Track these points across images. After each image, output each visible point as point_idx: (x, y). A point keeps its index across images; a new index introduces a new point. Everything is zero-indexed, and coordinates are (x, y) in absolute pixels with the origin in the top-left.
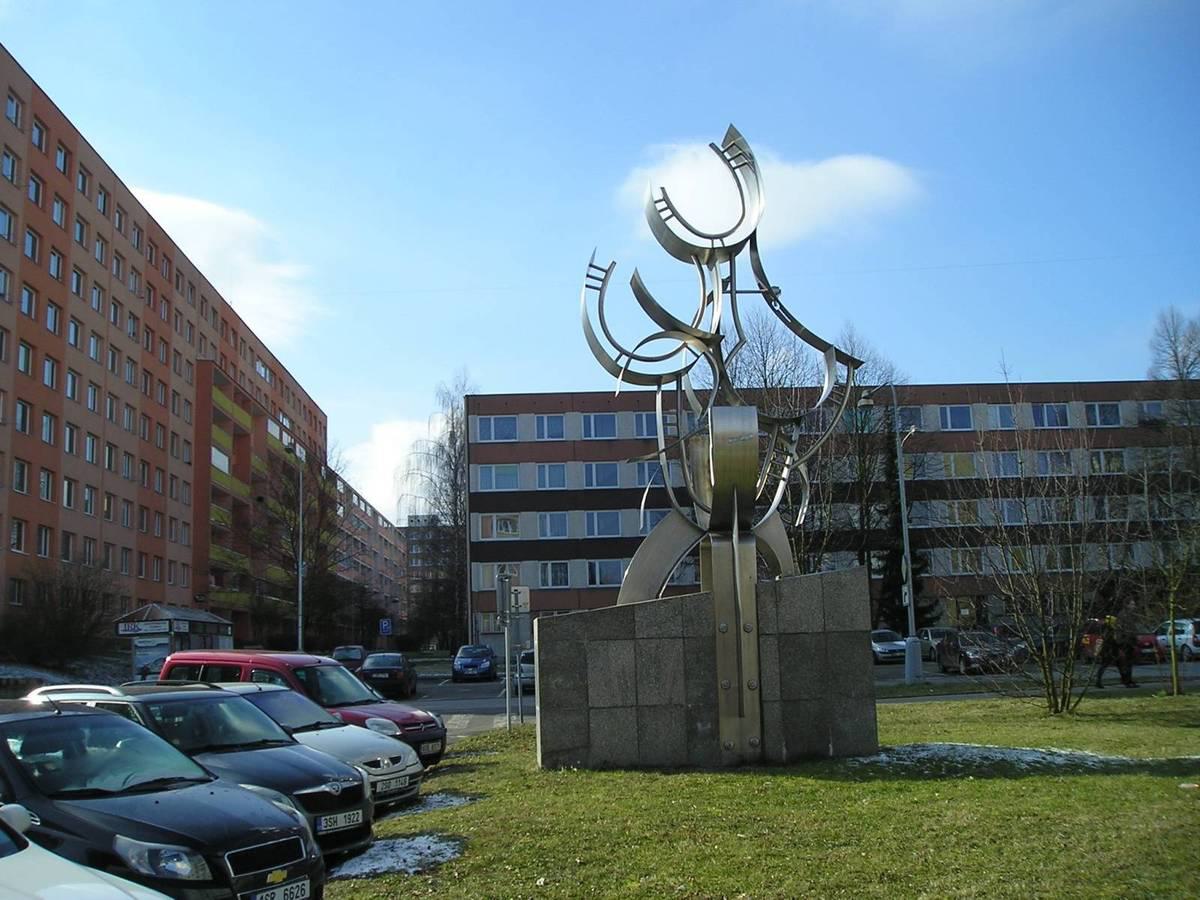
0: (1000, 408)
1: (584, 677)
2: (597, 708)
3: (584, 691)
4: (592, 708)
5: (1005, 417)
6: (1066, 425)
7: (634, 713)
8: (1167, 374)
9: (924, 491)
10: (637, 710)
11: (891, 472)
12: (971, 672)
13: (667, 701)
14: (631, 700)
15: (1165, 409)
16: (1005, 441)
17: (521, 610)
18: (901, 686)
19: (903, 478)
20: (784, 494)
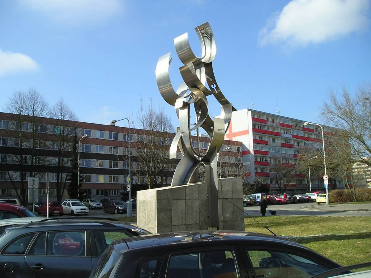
0: (100, 132)
1: (170, 214)
2: (174, 225)
3: (170, 219)
4: (173, 225)
5: (101, 135)
6: (118, 139)
7: (185, 226)
8: (149, 128)
9: (85, 156)
10: (186, 226)
11: (75, 148)
12: (118, 213)
13: (194, 222)
14: (184, 223)
15: (146, 138)
16: (100, 142)
17: (35, 187)
18: (126, 217)
19: (79, 150)
20: (326, 171)
